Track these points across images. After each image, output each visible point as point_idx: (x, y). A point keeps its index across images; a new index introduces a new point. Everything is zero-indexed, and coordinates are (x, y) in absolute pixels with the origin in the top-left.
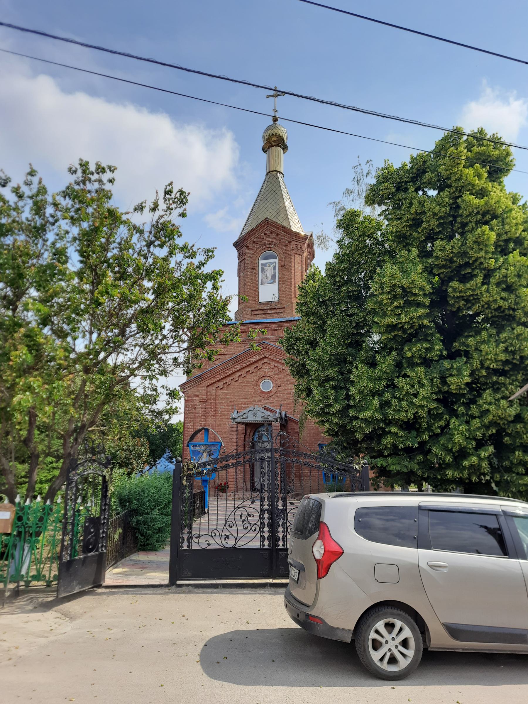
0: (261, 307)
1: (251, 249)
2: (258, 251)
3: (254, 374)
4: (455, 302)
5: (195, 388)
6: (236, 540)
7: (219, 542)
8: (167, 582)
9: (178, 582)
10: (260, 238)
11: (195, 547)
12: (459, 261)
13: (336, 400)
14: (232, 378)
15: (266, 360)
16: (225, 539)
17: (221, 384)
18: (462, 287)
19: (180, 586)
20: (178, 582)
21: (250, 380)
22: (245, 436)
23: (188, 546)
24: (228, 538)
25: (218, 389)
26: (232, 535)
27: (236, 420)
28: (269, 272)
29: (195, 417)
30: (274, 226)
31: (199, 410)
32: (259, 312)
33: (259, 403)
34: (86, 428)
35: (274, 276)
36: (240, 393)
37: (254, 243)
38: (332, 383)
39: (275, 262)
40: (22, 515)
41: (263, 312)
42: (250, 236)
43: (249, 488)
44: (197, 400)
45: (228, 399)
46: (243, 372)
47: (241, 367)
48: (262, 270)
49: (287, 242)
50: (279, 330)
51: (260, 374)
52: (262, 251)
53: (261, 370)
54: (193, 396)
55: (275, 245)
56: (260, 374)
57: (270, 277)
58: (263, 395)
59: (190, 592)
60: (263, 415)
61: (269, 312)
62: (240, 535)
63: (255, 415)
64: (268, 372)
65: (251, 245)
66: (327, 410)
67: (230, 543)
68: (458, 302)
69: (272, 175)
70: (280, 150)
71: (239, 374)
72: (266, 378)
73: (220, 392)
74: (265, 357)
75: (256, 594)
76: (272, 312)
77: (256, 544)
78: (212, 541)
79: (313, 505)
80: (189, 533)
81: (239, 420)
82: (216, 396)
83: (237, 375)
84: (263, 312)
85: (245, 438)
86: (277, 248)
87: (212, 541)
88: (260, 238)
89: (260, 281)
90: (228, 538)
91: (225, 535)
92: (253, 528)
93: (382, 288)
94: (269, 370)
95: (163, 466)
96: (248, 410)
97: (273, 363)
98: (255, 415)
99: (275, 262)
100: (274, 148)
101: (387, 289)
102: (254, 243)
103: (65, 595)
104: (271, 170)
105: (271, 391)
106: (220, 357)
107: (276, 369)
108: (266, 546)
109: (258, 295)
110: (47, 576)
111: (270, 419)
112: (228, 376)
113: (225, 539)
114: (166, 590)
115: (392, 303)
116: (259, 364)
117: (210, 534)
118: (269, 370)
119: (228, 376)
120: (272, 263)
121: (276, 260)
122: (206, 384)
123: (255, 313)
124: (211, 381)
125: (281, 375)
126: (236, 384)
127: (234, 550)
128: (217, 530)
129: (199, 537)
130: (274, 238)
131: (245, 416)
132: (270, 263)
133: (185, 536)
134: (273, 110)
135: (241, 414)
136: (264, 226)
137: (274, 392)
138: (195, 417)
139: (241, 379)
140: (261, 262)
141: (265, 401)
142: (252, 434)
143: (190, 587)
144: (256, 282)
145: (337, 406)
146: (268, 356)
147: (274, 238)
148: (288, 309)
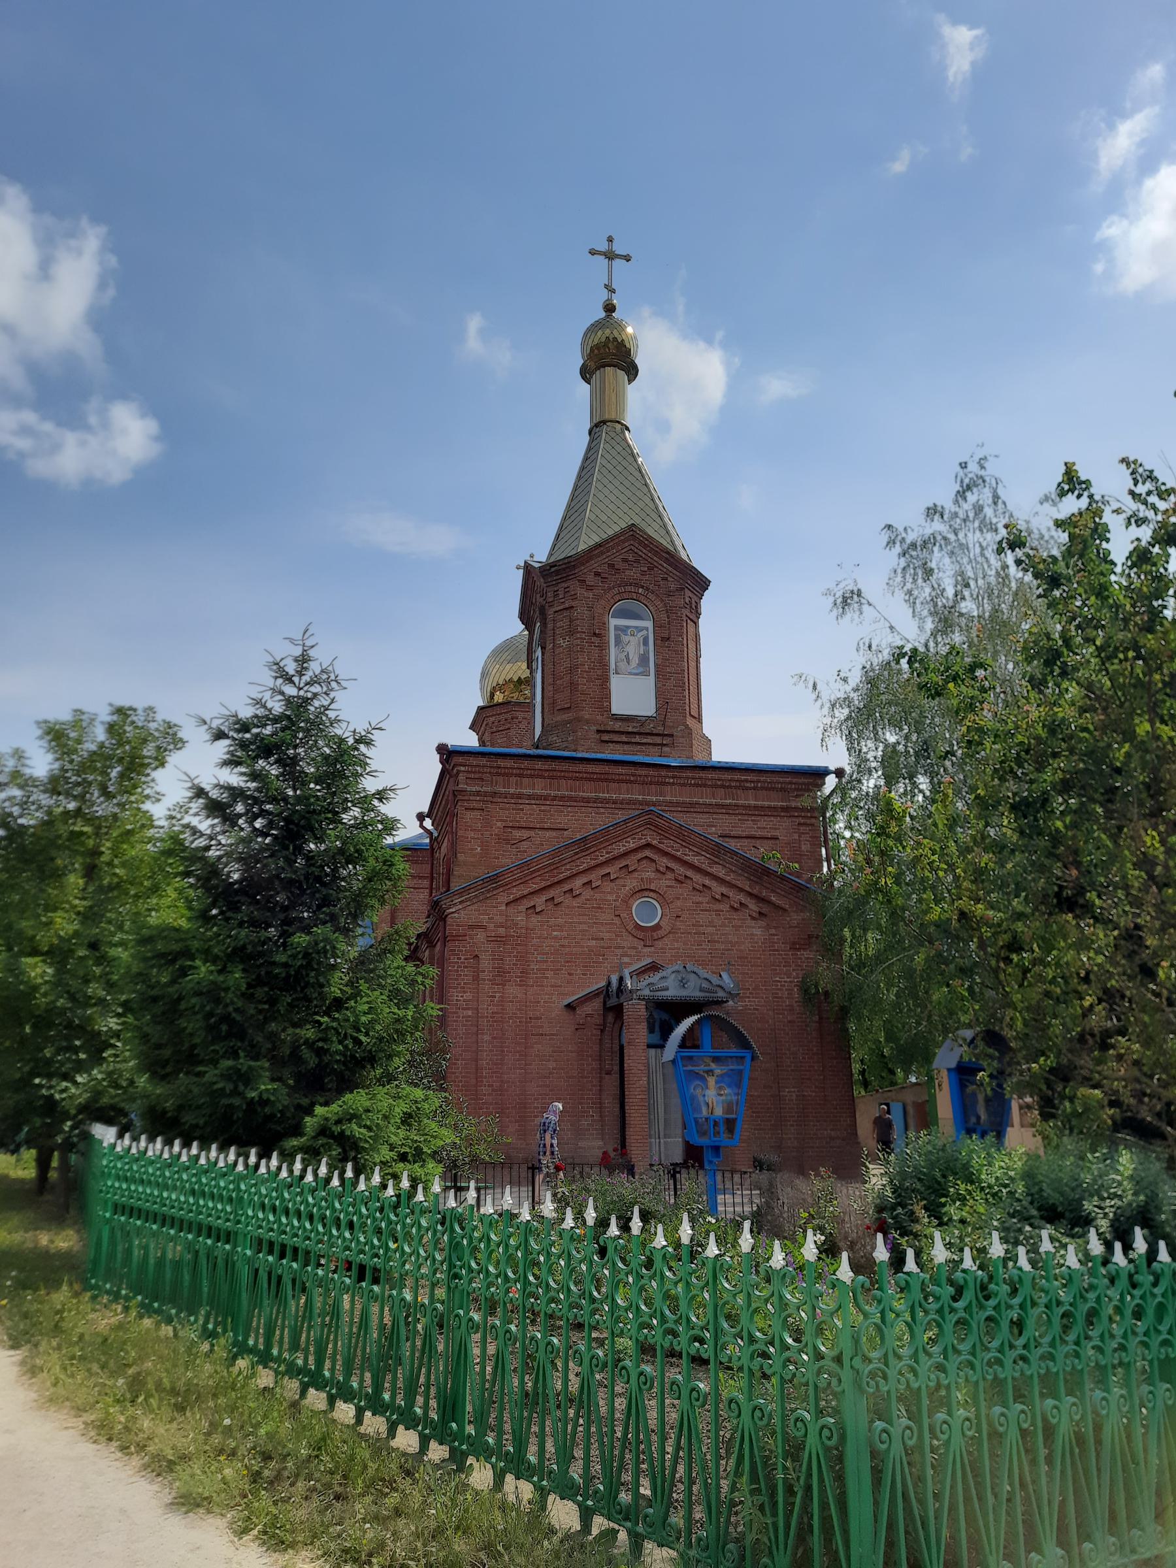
0: (618, 726)
1: (590, 588)
2: (609, 596)
3: (617, 882)
5: (475, 907)
10: (611, 566)
14: (567, 887)
15: (647, 853)
21: (609, 897)
28: (633, 647)
29: (476, 978)
30: (645, 546)
31: (486, 963)
32: (616, 738)
33: (633, 952)
35: (644, 660)
36: (585, 927)
37: (597, 574)
39: (647, 629)
41: (624, 738)
42: (591, 558)
44: (481, 936)
45: (556, 938)
47: (593, 863)
48: (618, 641)
49: (673, 586)
50: (673, 784)
51: (631, 883)
52: (618, 597)
53: (636, 875)
54: (472, 927)
55: (648, 589)
56: (631, 883)
57: (635, 660)
58: (641, 935)
61: (638, 739)
63: (683, 984)
64: (650, 881)
65: (590, 579)
69: (605, 426)
70: (622, 375)
71: (585, 880)
72: (646, 894)
73: (535, 919)
74: (648, 845)
76: (645, 741)
79: (503, 1193)
81: (647, 992)
83: (578, 882)
84: (624, 738)
86: (650, 596)
88: (611, 566)
89: (613, 666)
97: (664, 861)
99: (647, 629)
100: (609, 370)
102: (597, 574)
103: (1073, 1503)
104: (607, 417)
105: (657, 927)
106: (532, 833)
107: (670, 875)
109: (608, 697)
112: (559, 882)
116: (631, 861)
118: (653, 875)
119: (559, 882)
120: (640, 629)
121: (649, 624)
122: (504, 898)
123: (606, 737)
124: (517, 892)
130: (643, 573)
132: (636, 627)
134: (606, 286)
136: (623, 541)
137: (668, 929)
138: (476, 978)
139: (587, 893)
140: (614, 622)
144: (604, 665)
146: (654, 842)
147: (643, 573)
148: (681, 740)
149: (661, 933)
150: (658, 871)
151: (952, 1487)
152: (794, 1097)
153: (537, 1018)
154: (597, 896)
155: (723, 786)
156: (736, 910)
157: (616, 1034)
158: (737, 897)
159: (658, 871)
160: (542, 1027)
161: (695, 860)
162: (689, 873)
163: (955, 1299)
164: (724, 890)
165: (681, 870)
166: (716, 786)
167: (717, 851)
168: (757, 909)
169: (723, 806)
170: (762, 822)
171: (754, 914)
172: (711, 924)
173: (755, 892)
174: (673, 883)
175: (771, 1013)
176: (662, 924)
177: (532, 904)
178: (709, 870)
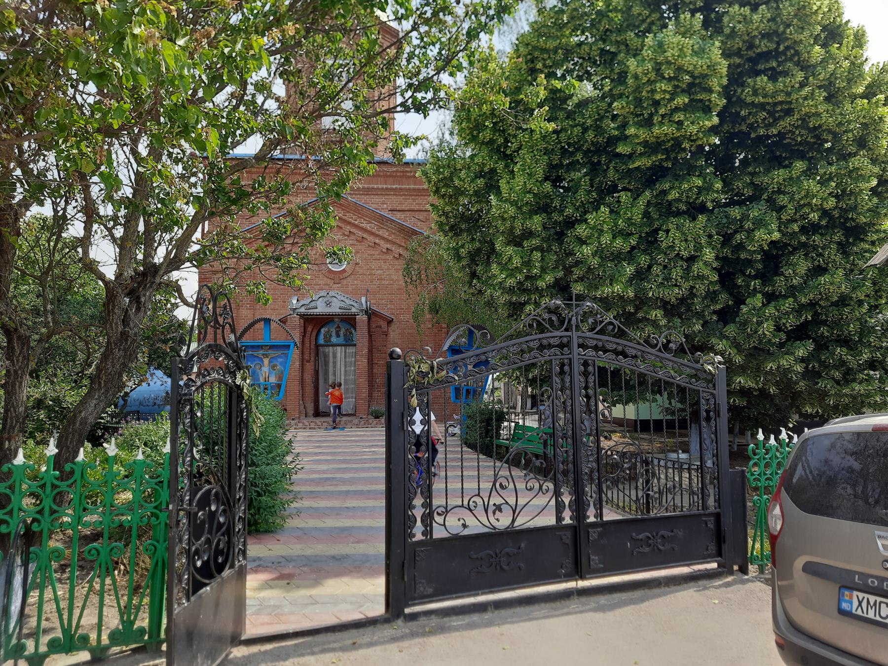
4: (750, 113)
6: (514, 512)
7: (484, 519)
8: (379, 609)
9: (407, 611)
11: (439, 533)
12: (764, 46)
13: (544, 270)
16: (494, 513)
18: (770, 87)
19: (414, 617)
20: (407, 611)
22: (304, 336)
23: (423, 534)
24: (500, 510)
26: (507, 503)
34: (161, 273)
38: (535, 242)
40: (8, 491)
43: (311, 411)
58: (332, 276)
59: (442, 630)
60: (342, 305)
62: (522, 501)
63: (328, 304)
66: (528, 284)
67: (503, 521)
68: (756, 114)
75: (567, 614)
77: (548, 520)
78: (471, 521)
80: (428, 505)
81: (303, 310)
87: (471, 521)
90: (500, 510)
91: (495, 504)
92: (544, 487)
93: (658, 69)
95: (159, 383)
98: (328, 304)
101: (669, 72)
107: (352, 237)
108: (567, 521)
110: (93, 636)
111: (354, 310)
113: (494, 513)
114: (387, 631)
115: (672, 99)
117: (466, 503)
127: (512, 535)
128: (479, 495)
129: (446, 511)
131: (313, 304)
133: (418, 512)
135: (306, 301)
141: (334, 286)
142: (314, 334)
143: (433, 617)
145: (549, 278)
149: (346, 275)
150: (344, 235)
151: (364, 509)
155: (391, 176)
156: (397, 259)
157: (313, 338)
159: (344, 235)
161: (368, 227)
163: (766, 454)
164: (389, 246)
166: (387, 176)
167: (382, 220)
169: (392, 189)
170: (419, 200)
172: (380, 268)
174: (355, 242)
176: (347, 269)
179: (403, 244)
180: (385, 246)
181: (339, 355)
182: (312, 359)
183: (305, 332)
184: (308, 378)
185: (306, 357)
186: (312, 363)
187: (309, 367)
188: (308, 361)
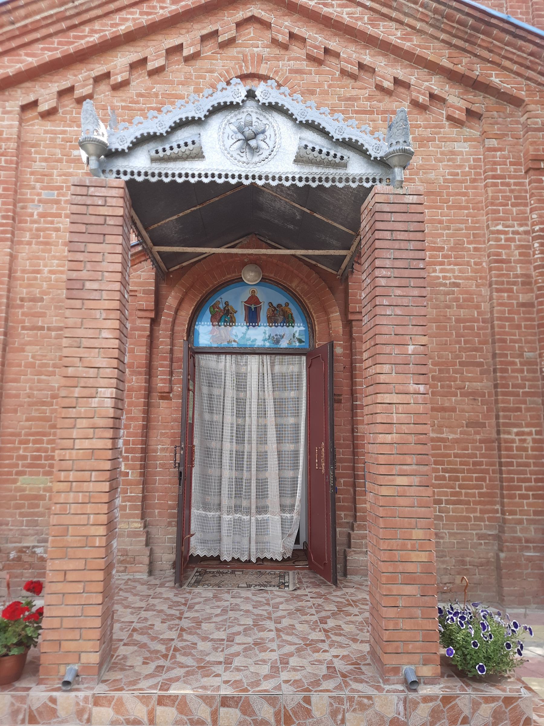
3: (198, 63)
14: (99, 68)
17: (46, 93)
22: (154, 322)
25: (30, 114)
27: (121, 164)
43: (166, 557)
46: (154, 50)
47: (144, 20)
53: (233, 51)
63: (249, 140)
64: (261, 59)
73: (38, 129)
81: (140, 163)
82: (21, 143)
83: (119, 62)
85: (152, 330)
94: (266, 52)
96: (208, 104)
107: (297, 50)
125: (317, 78)
126: (118, 100)
131: (184, 136)
139: (140, 83)
142: (185, 314)
150: (275, 42)
152: (529, 444)
153: (34, 300)
154: (158, 88)
157: (182, 327)
158: (425, 84)
160: (42, 315)
162: (334, 44)
164: (401, 73)
165: (317, 38)
168: (463, 104)
171: (457, 114)
173: (460, 69)
174: (304, 65)
175: (485, 291)
177: (32, 98)
178: (371, 30)
179: (445, 63)
180: (387, 70)
181: (253, 382)
182: (178, 388)
183: (158, 308)
184: (163, 448)
185: (160, 384)
186: (177, 402)
187: (166, 412)
188: (165, 396)
